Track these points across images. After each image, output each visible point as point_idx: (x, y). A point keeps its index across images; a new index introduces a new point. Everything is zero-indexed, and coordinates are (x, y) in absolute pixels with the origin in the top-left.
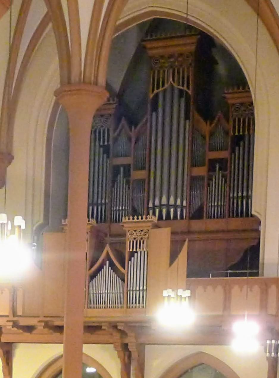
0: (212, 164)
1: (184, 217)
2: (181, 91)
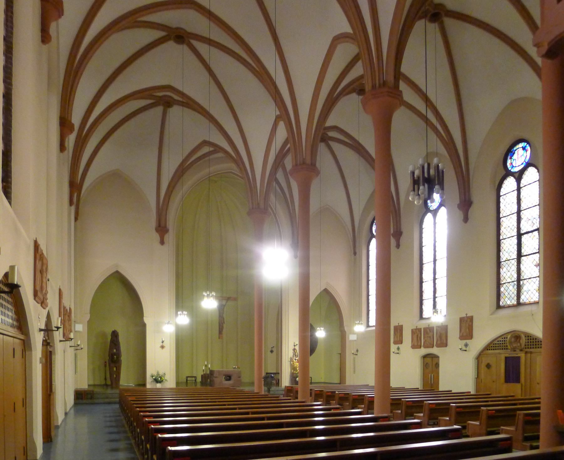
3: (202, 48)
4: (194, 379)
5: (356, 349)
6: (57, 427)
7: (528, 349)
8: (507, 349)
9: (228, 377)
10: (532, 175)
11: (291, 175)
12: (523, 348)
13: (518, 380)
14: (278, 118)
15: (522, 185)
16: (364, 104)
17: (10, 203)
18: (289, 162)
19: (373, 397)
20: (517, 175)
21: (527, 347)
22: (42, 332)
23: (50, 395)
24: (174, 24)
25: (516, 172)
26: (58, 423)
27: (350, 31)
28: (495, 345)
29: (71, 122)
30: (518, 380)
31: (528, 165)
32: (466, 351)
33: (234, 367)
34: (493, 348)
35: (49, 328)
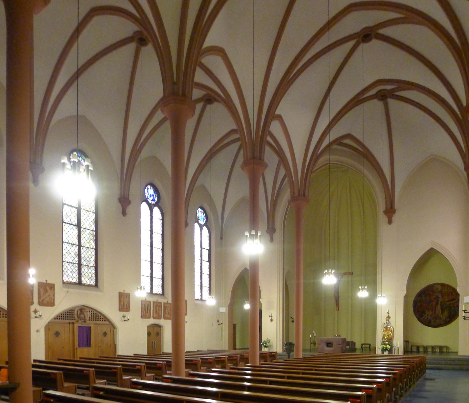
4: (368, 346)
5: (217, 320)
7: (99, 322)
19: (170, 362)
20: (153, 206)
21: (60, 318)
33: (335, 335)
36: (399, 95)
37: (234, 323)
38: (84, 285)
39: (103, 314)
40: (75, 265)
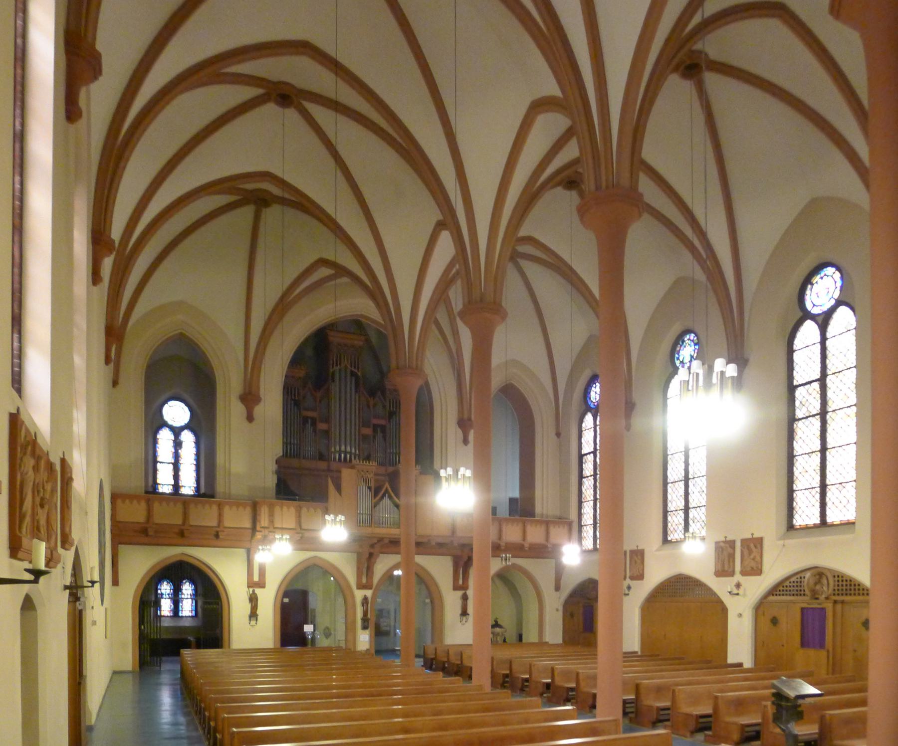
0: (375, 427)
1: (332, 459)
2: (352, 372)
3: (314, 109)
6: (90, 729)
8: (804, 595)
9: (364, 640)
10: (844, 318)
11: (461, 319)
12: (830, 595)
13: (821, 644)
14: (440, 226)
15: (828, 335)
16: (582, 211)
17: (20, 397)
18: (457, 297)
20: (820, 319)
22: (68, 591)
23: (80, 684)
24: (275, 76)
25: (819, 315)
26: (91, 721)
27: (558, 93)
28: (785, 588)
29: (109, 237)
30: (821, 644)
31: (839, 303)
32: (738, 594)
34: (781, 593)
35: (79, 584)
36: (310, 111)
37: (91, 566)
38: (833, 525)
39: (792, 573)
40: (813, 491)
